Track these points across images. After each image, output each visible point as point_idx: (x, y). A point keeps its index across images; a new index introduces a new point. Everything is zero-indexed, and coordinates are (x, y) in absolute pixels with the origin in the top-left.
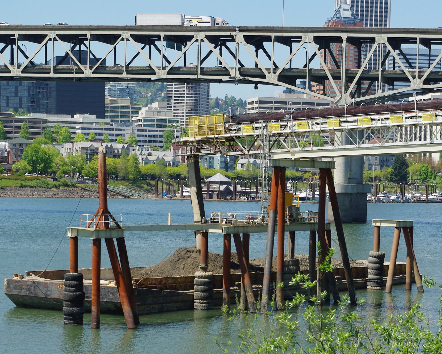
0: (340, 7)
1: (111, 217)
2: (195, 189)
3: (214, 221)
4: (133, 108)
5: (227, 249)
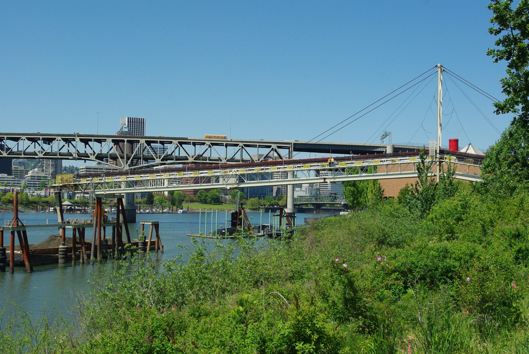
0: (123, 127)
1: (20, 221)
2: (59, 208)
3: (68, 223)
4: (25, 171)
5: (74, 235)
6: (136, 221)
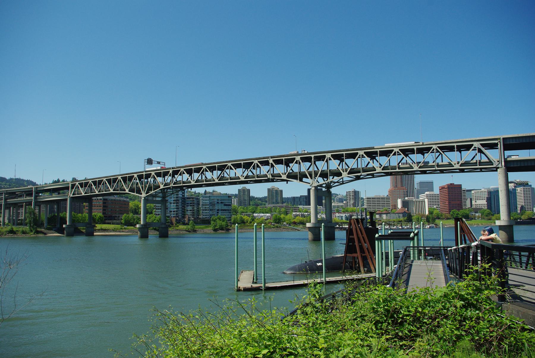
6: (336, 237)
